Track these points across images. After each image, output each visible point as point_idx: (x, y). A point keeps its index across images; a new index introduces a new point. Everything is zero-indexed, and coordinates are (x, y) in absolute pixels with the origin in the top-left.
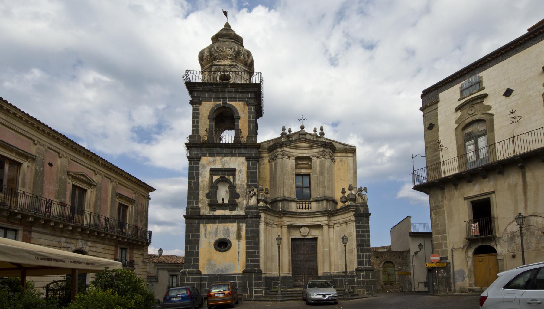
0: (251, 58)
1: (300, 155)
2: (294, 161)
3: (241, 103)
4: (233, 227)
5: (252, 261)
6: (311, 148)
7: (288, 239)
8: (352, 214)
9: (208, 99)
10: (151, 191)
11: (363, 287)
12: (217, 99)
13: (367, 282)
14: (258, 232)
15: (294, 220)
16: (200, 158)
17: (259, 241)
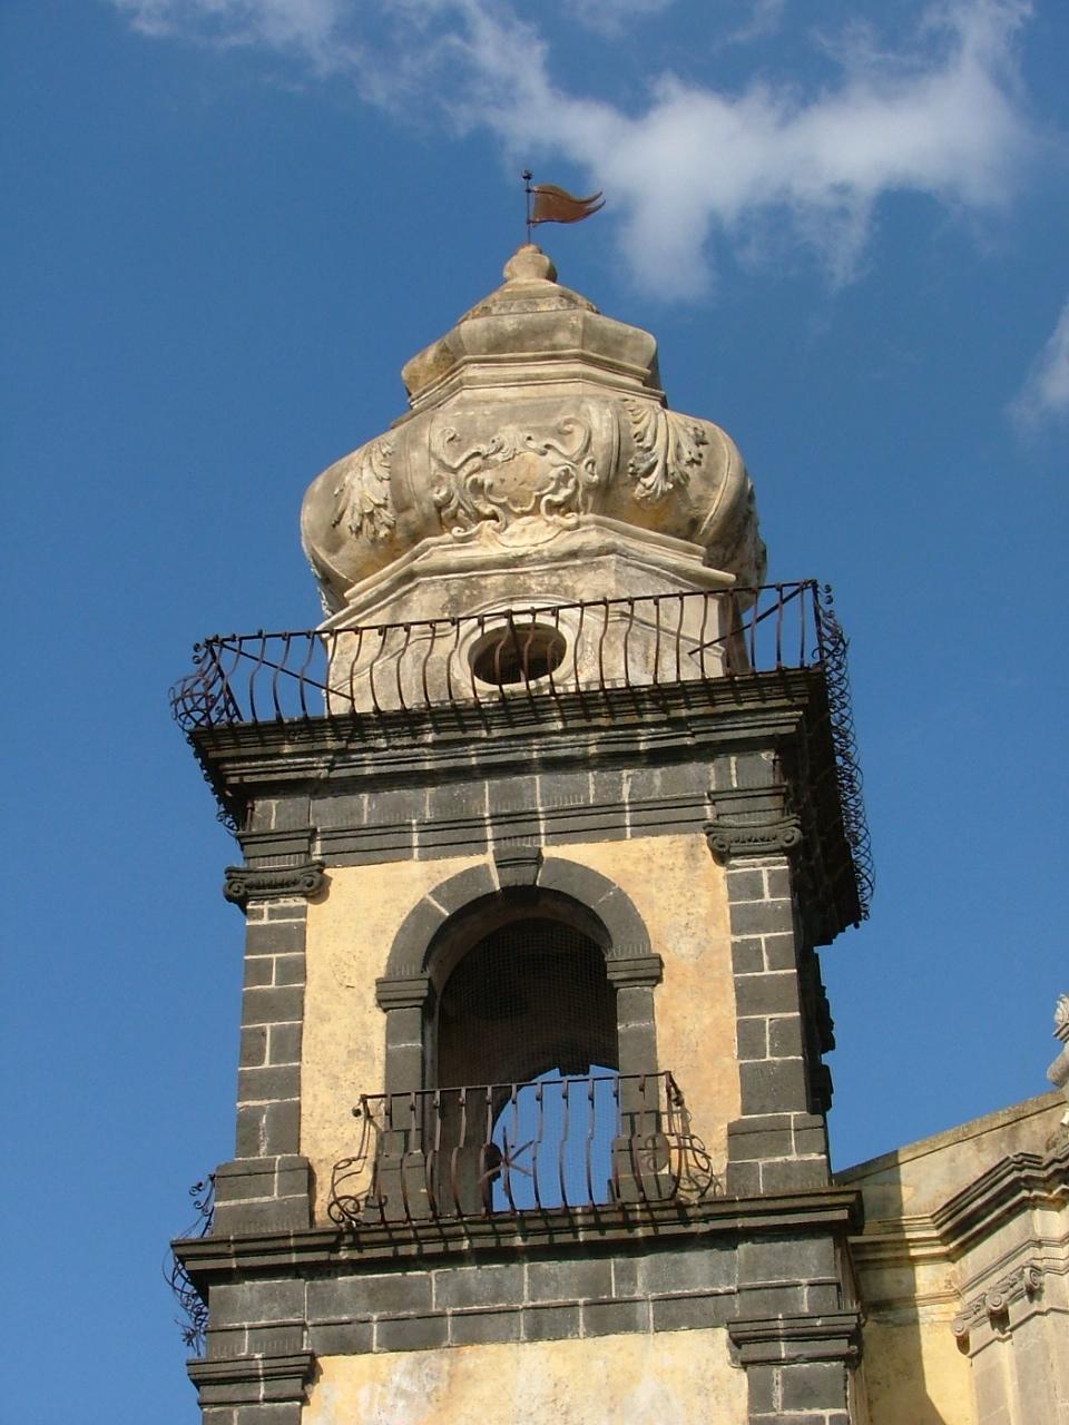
3: (660, 843)
9: (382, 844)
12: (454, 832)
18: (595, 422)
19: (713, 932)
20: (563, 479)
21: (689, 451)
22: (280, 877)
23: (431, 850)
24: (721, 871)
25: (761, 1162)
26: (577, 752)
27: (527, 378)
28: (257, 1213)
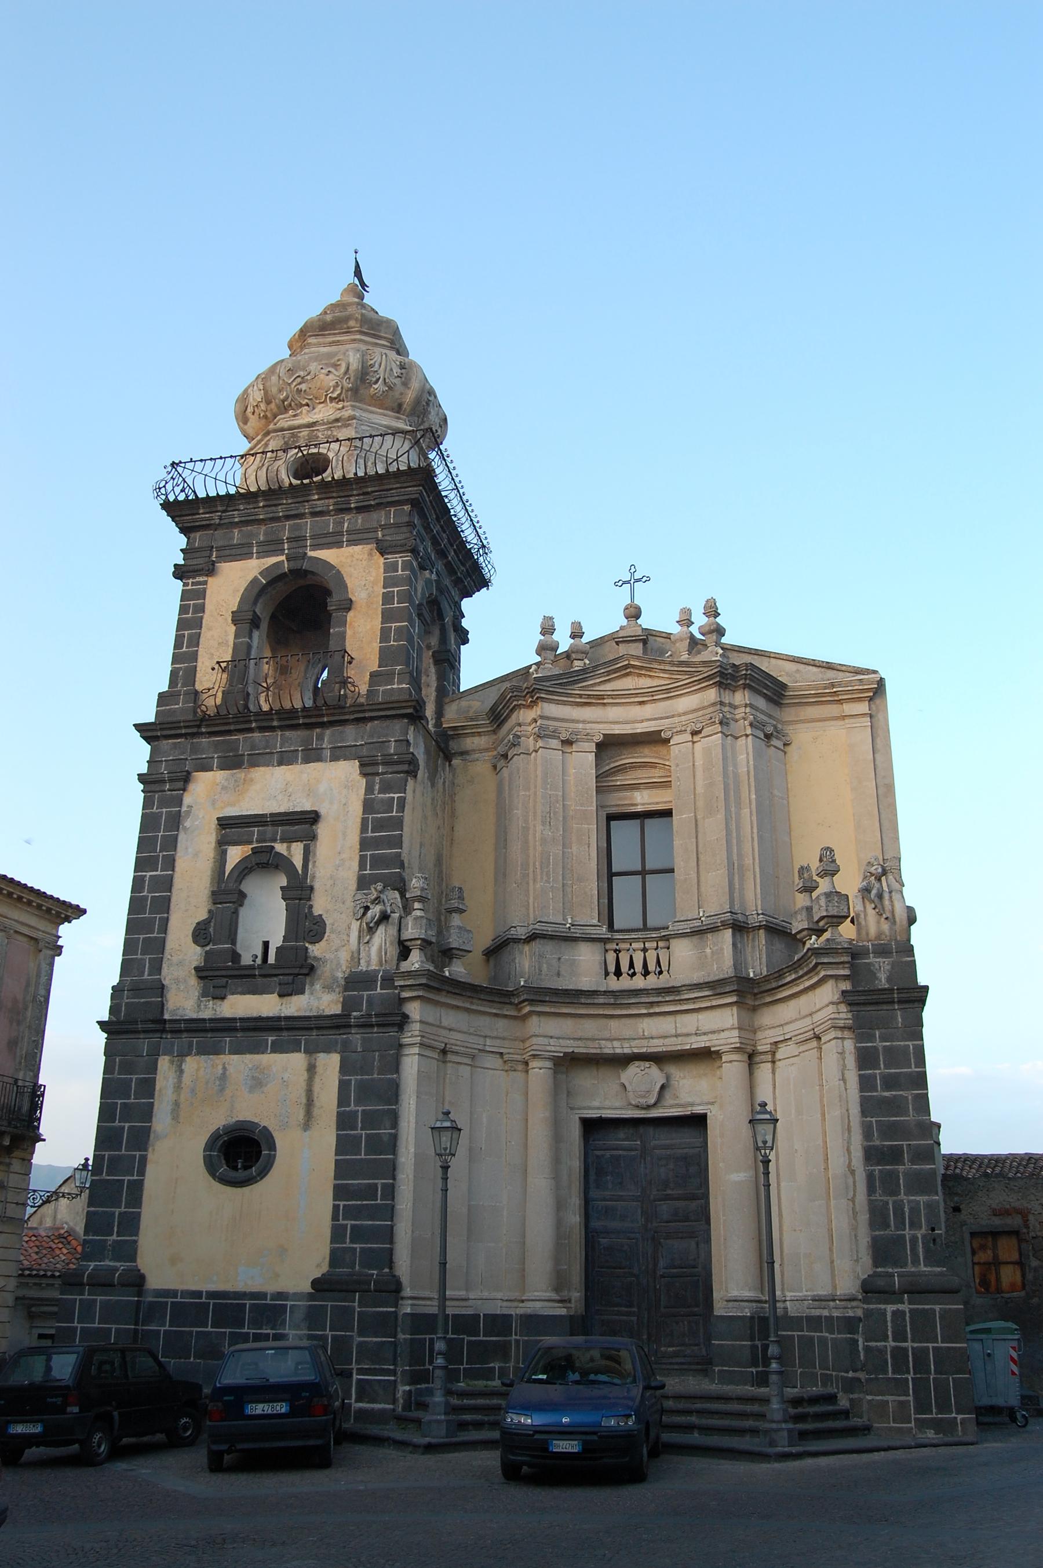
0: (415, 385)
1: (617, 730)
2: (591, 757)
3: (358, 548)
4: (288, 1066)
5: (358, 1234)
6: (669, 693)
7: (556, 1125)
8: (828, 993)
9: (241, 553)
10: (68, 919)
11: (900, 1387)
12: (271, 547)
13: (921, 1357)
14: (392, 1093)
15: (589, 1028)
16: (186, 779)
17: (394, 1138)
18: (351, 360)
19: (375, 588)
20: (337, 385)
21: (396, 371)
22: (196, 567)
23: (262, 554)
24: (382, 560)
25: (381, 689)
26: (325, 509)
27: (334, 342)
28: (175, 711)
